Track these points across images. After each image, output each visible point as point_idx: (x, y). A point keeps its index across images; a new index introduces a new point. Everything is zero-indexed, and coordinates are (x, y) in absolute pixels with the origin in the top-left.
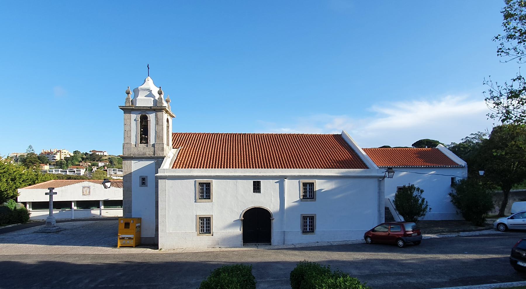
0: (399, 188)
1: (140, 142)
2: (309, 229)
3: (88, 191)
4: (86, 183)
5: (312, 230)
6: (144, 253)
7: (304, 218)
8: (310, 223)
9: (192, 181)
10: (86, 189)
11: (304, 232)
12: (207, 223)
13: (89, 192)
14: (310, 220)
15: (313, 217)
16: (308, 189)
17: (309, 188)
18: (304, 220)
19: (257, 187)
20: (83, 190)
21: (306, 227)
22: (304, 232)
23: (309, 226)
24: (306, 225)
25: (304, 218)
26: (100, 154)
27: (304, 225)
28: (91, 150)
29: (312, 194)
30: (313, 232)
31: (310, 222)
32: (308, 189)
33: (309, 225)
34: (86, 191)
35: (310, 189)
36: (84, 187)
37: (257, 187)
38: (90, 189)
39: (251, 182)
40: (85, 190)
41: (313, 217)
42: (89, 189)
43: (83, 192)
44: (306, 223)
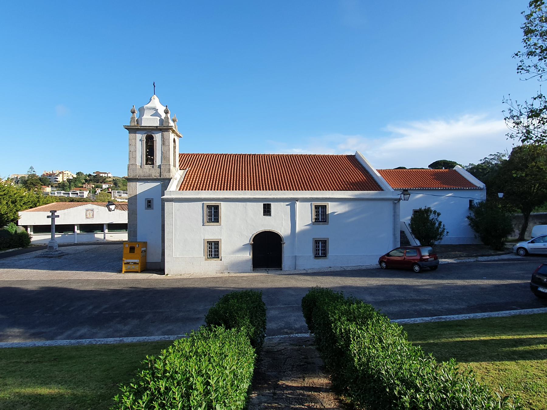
0: (415, 211)
1: (146, 163)
2: (322, 253)
3: (91, 214)
4: (89, 206)
5: (325, 255)
6: (149, 278)
7: (317, 242)
8: (322, 247)
9: (200, 204)
11: (317, 256)
12: (215, 247)
13: (93, 215)
14: (322, 244)
15: (326, 241)
16: (320, 212)
17: (322, 211)
18: (316, 244)
19: (267, 210)
20: (86, 213)
21: (318, 251)
22: (317, 256)
23: (322, 251)
24: (318, 249)
25: (317, 242)
26: (104, 175)
27: (316, 250)
28: (95, 172)
29: (325, 217)
30: (326, 256)
31: (322, 246)
32: (320, 212)
33: (322, 249)
34: (89, 214)
35: (322, 212)
36: (87, 210)
37: (267, 210)
38: (93, 212)
39: (261, 205)
40: (88, 213)
41: (326, 241)
43: (86, 215)
44: (318, 247)
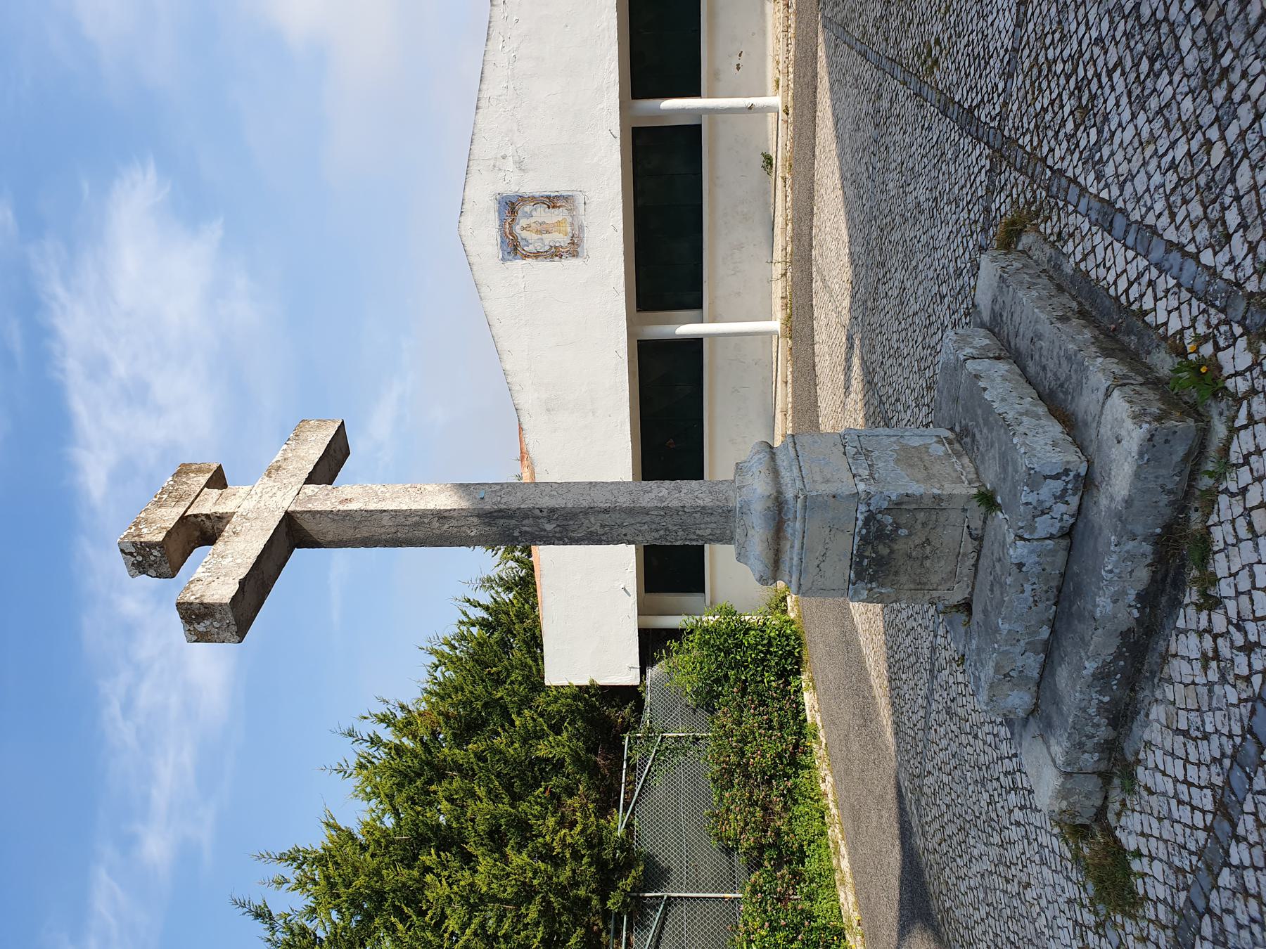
3: (542, 214)
10: (523, 229)
13: (551, 202)
20: (537, 255)
34: (543, 230)
38: (523, 199)
40: (533, 241)
42: (528, 208)
